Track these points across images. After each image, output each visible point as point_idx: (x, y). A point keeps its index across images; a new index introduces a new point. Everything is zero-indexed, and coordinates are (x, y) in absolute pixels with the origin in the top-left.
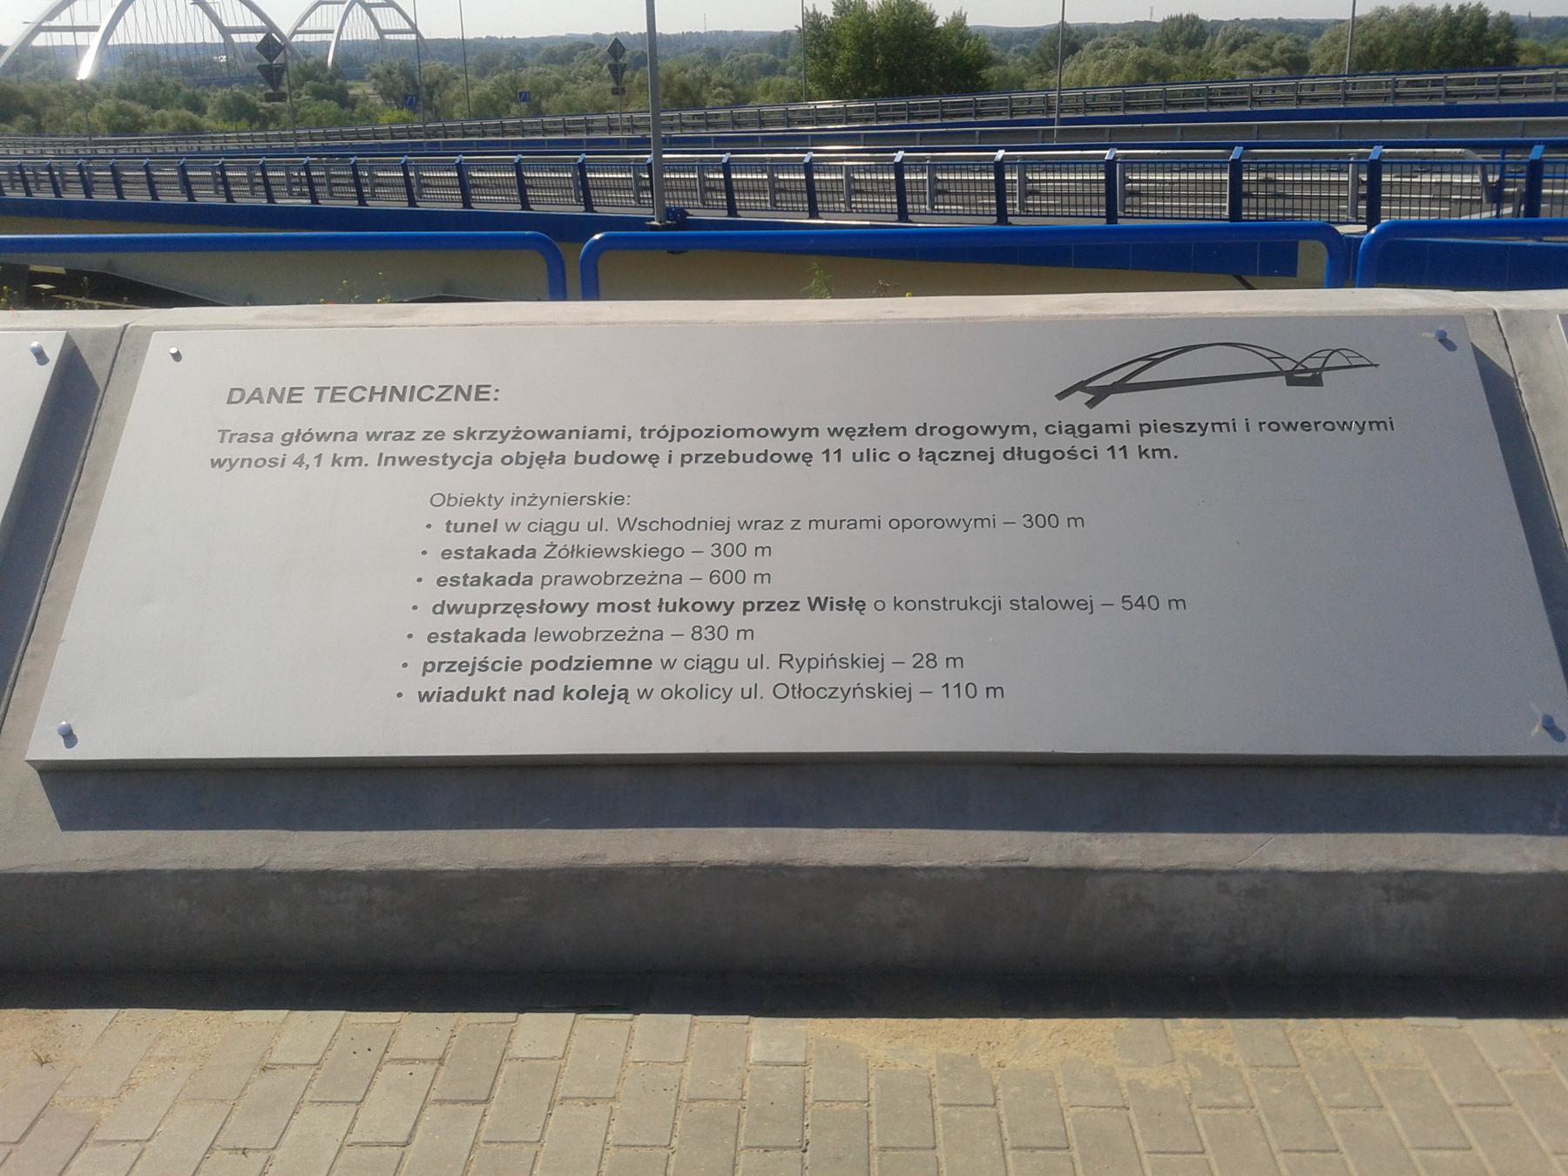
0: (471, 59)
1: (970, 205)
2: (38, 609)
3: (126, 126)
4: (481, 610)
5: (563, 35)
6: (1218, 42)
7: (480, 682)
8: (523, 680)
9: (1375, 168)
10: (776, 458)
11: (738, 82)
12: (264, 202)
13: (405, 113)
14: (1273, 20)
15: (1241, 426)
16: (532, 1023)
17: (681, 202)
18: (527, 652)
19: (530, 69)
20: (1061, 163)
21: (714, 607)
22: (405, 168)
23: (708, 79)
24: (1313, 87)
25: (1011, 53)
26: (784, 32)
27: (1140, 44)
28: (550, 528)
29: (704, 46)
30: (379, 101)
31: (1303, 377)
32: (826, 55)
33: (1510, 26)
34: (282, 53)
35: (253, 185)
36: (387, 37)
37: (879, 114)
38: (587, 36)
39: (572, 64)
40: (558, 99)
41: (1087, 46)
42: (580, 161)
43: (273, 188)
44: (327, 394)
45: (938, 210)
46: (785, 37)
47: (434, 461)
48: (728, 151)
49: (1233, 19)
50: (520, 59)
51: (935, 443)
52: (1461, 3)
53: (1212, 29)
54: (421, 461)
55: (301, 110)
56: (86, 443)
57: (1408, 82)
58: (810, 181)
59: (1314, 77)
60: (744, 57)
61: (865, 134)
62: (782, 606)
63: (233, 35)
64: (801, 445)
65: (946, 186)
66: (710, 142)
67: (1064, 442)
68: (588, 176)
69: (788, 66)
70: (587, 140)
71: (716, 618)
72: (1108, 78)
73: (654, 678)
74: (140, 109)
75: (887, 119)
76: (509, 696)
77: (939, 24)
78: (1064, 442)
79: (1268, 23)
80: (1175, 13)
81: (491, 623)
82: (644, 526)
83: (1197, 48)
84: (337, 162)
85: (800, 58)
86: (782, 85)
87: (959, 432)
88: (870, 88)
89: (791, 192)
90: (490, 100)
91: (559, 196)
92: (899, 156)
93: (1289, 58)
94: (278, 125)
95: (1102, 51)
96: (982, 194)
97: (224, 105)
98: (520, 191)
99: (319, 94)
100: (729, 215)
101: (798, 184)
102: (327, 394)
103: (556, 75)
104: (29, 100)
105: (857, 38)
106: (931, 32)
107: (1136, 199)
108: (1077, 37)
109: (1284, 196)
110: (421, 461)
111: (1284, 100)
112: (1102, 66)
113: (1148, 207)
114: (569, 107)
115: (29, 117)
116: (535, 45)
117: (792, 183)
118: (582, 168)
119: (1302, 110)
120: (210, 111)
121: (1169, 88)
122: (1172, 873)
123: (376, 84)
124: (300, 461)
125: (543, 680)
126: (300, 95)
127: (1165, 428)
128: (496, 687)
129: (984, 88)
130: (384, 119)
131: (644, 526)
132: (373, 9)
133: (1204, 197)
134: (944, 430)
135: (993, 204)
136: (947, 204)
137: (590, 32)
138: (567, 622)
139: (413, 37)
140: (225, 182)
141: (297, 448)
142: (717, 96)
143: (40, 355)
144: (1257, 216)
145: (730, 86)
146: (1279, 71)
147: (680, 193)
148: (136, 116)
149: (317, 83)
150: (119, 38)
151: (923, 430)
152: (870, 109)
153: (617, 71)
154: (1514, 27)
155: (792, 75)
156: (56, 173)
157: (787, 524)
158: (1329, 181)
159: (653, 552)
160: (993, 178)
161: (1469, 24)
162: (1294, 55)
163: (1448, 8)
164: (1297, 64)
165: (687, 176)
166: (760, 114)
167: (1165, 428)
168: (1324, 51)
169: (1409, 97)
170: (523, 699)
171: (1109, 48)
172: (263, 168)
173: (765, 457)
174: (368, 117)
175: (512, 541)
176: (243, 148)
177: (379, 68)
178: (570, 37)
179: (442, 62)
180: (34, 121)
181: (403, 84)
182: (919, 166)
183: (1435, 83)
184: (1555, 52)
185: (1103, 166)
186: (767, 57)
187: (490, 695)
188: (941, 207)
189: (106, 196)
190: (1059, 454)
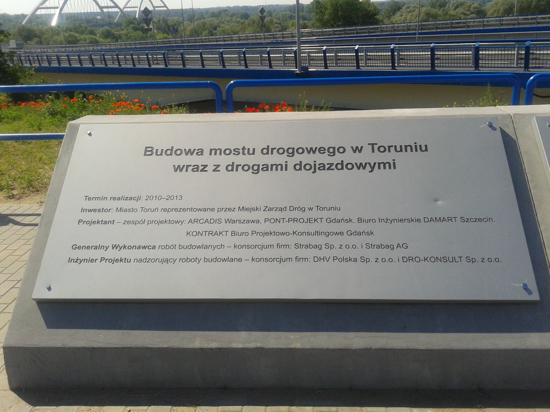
0: (185, 16)
1: (290, 63)
2: (542, 234)
3: (73, 41)
5: (216, 7)
6: (451, 5)
9: (477, 49)
12: (472, 70)
13: (165, 35)
17: (305, 65)
20: (505, 47)
22: (147, 55)
23: (272, 22)
24: (488, 21)
32: (321, 12)
34: (151, 14)
35: (240, 60)
36: (156, 9)
41: (404, 8)
42: (221, 51)
43: (94, 61)
45: (400, 65)
50: (202, 16)
55: (129, 35)
56: (523, 163)
57: (524, 18)
58: (325, 56)
59: (488, 18)
61: (335, 40)
65: (403, 57)
66: (250, 45)
68: (224, 56)
70: (224, 44)
83: (443, 7)
88: (337, 23)
89: (343, 60)
90: (195, 30)
91: (214, 63)
92: (357, 47)
93: (477, 11)
94: (122, 40)
95: (409, 9)
96: (410, 59)
97: (103, 33)
98: (431, 61)
99: (135, 29)
100: (270, 68)
101: (321, 58)
104: (38, 33)
106: (358, 3)
107: (340, 61)
109: (539, 59)
111: (477, 26)
112: (413, 15)
113: (410, 63)
114: (224, 32)
115: (38, 39)
116: (207, 11)
117: (346, 57)
118: (222, 53)
119: (485, 29)
121: (437, 22)
133: (504, 59)
135: (355, 63)
136: (404, 63)
140: (105, 60)
144: (440, 65)
145: (280, 24)
146: (474, 15)
147: (255, 61)
148: (76, 38)
149: (134, 25)
150: (66, 10)
152: (342, 31)
156: (49, 58)
158: (511, 53)
160: (390, 54)
165: (380, 54)
168: (492, 8)
169: (522, 24)
170: (135, 249)
172: (244, 53)
176: (117, 48)
178: (218, 8)
179: (177, 17)
180: (39, 40)
181: (163, 25)
182: (331, 51)
183: (532, 19)
185: (267, 52)
186: (289, 13)
188: (401, 64)
189: (65, 65)
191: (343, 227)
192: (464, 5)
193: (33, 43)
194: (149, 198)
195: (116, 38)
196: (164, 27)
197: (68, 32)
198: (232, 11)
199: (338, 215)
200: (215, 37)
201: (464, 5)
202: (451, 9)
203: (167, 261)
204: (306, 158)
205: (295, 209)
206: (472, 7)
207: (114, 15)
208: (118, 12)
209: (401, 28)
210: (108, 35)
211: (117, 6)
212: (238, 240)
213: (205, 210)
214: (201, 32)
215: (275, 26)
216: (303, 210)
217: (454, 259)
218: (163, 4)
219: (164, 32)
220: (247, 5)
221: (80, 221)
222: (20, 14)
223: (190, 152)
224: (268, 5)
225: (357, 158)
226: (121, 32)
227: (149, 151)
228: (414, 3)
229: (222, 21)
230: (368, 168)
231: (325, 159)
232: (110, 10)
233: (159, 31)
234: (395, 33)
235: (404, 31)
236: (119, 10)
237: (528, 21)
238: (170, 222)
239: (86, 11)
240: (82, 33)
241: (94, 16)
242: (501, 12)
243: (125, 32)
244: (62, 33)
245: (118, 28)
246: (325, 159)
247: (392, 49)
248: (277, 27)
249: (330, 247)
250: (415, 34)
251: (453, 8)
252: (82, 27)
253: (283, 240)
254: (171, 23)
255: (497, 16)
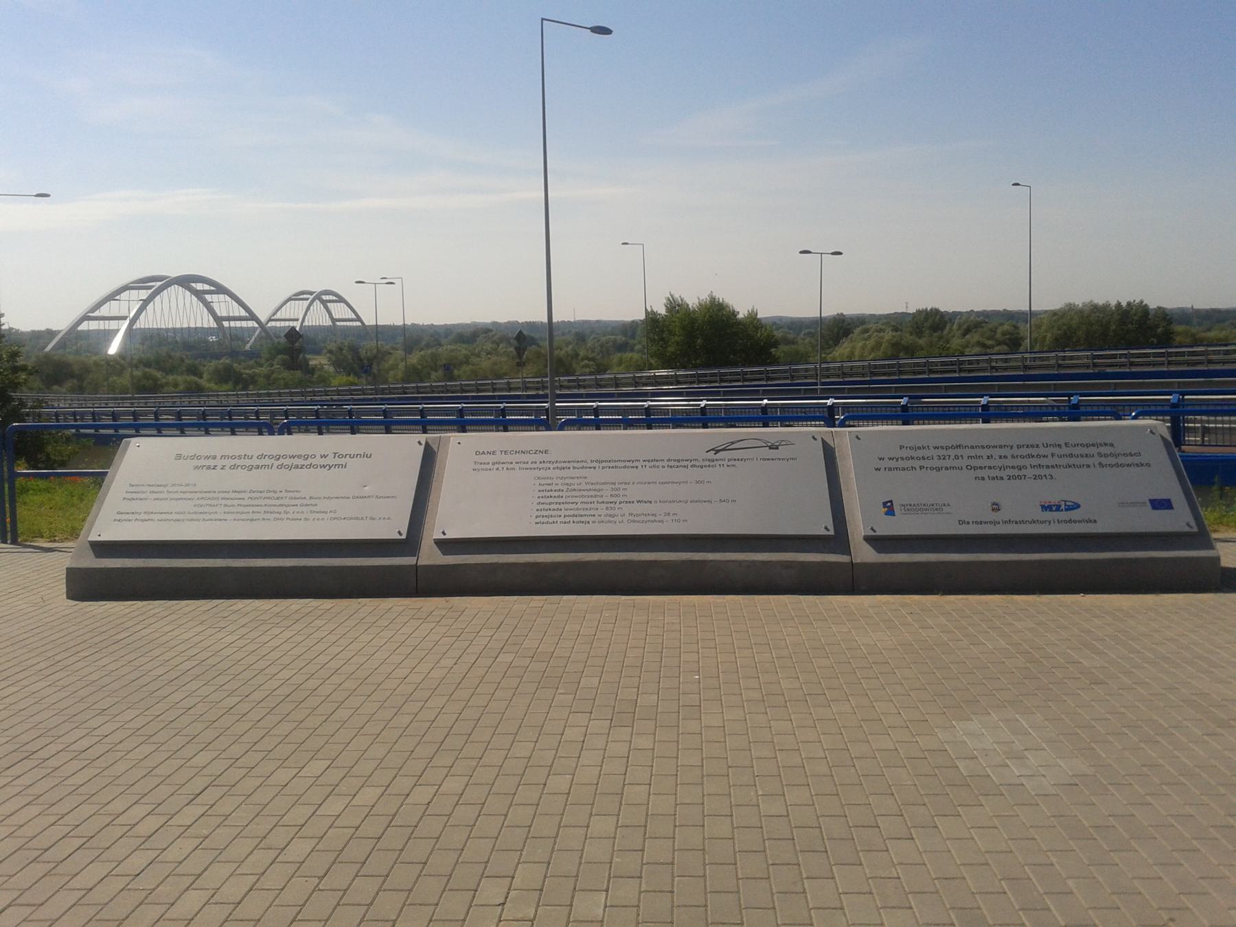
4: (550, 504)
6: (955, 327)
7: (551, 520)
8: (562, 519)
10: (628, 467)
11: (599, 357)
13: (351, 378)
14: (999, 311)
15: (755, 459)
16: (565, 597)
18: (562, 513)
19: (445, 347)
21: (611, 503)
23: (577, 355)
25: (802, 336)
26: (633, 321)
27: (896, 329)
28: (567, 484)
29: (574, 331)
30: (332, 369)
31: (773, 447)
32: (662, 339)
33: (1165, 316)
36: (338, 323)
37: (700, 379)
38: (487, 324)
39: (475, 344)
40: (466, 368)
41: (857, 331)
44: (503, 453)
46: (634, 325)
47: (535, 469)
48: (597, 401)
49: (968, 310)
51: (672, 463)
52: (1128, 300)
53: (950, 319)
54: (531, 469)
60: (603, 339)
61: (724, 391)
62: (630, 502)
63: (224, 323)
64: (635, 464)
67: (707, 463)
69: (635, 345)
71: (612, 505)
72: (870, 354)
73: (596, 519)
74: (159, 374)
75: (706, 382)
76: (559, 523)
77: (740, 316)
78: (707, 463)
79: (996, 314)
80: (922, 307)
81: (552, 507)
82: (592, 484)
84: (335, 409)
85: (644, 340)
86: (631, 358)
87: (679, 461)
88: (693, 362)
93: (1010, 339)
95: (868, 334)
102: (503, 453)
103: (464, 352)
105: (684, 328)
106: (735, 323)
108: (849, 324)
110: (531, 469)
114: (475, 375)
116: (448, 330)
120: (205, 376)
122: (728, 561)
123: (330, 358)
124: (497, 469)
125: (567, 519)
126: (273, 365)
127: (735, 460)
128: (555, 521)
129: (775, 361)
130: (335, 382)
131: (592, 484)
132: (329, 304)
134: (675, 460)
137: (489, 321)
138: (574, 506)
139: (358, 324)
141: (496, 466)
142: (583, 367)
143: (420, 443)
145: (593, 359)
148: (155, 380)
150: (141, 324)
151: (668, 460)
153: (520, 351)
154: (1168, 317)
155: (640, 351)
157: (631, 483)
159: (595, 490)
161: (1135, 315)
162: (1012, 337)
163: (1119, 305)
164: (1014, 343)
166: (524, 383)
167: (735, 460)
171: (873, 332)
173: (625, 467)
174: (324, 380)
175: (557, 488)
177: (333, 346)
178: (475, 325)
181: (350, 357)
184: (1203, 335)
186: (620, 339)
187: (554, 523)
190: (706, 466)
191: (299, 502)
192: (983, 327)
193: (64, 390)
194: (173, 485)
195: (241, 382)
196: (350, 361)
197: (141, 367)
198: (501, 331)
199: (298, 495)
200: (458, 383)
201: (983, 327)
202: (956, 336)
203: (179, 520)
204: (288, 462)
205: (270, 491)
206: (999, 331)
207: (246, 334)
208: (254, 329)
209: (832, 371)
210: (227, 376)
211: (253, 317)
212: (227, 509)
213: (209, 492)
214: (429, 374)
215: (582, 363)
216: (275, 492)
217: (362, 519)
218: (353, 314)
219: (350, 371)
220: (534, 320)
221: (124, 498)
222: (43, 329)
223: (207, 457)
224: (579, 321)
225: (324, 461)
226: (257, 371)
227: (179, 457)
228: (877, 323)
229: (477, 351)
230: (328, 467)
231: (300, 462)
232: (238, 324)
233: (338, 370)
234: (846, 379)
235: (863, 377)
236: (256, 325)
237: (1182, 358)
238: (185, 499)
239: (185, 326)
240: (171, 370)
241: (203, 336)
242: (1047, 342)
243: (264, 370)
244: (130, 370)
245: (251, 362)
246: (300, 462)
247: (903, 405)
248: (587, 366)
249: (287, 513)
250: (816, 384)
251: (959, 332)
252: (173, 358)
253: (256, 509)
254: (366, 353)
255: (1041, 350)
